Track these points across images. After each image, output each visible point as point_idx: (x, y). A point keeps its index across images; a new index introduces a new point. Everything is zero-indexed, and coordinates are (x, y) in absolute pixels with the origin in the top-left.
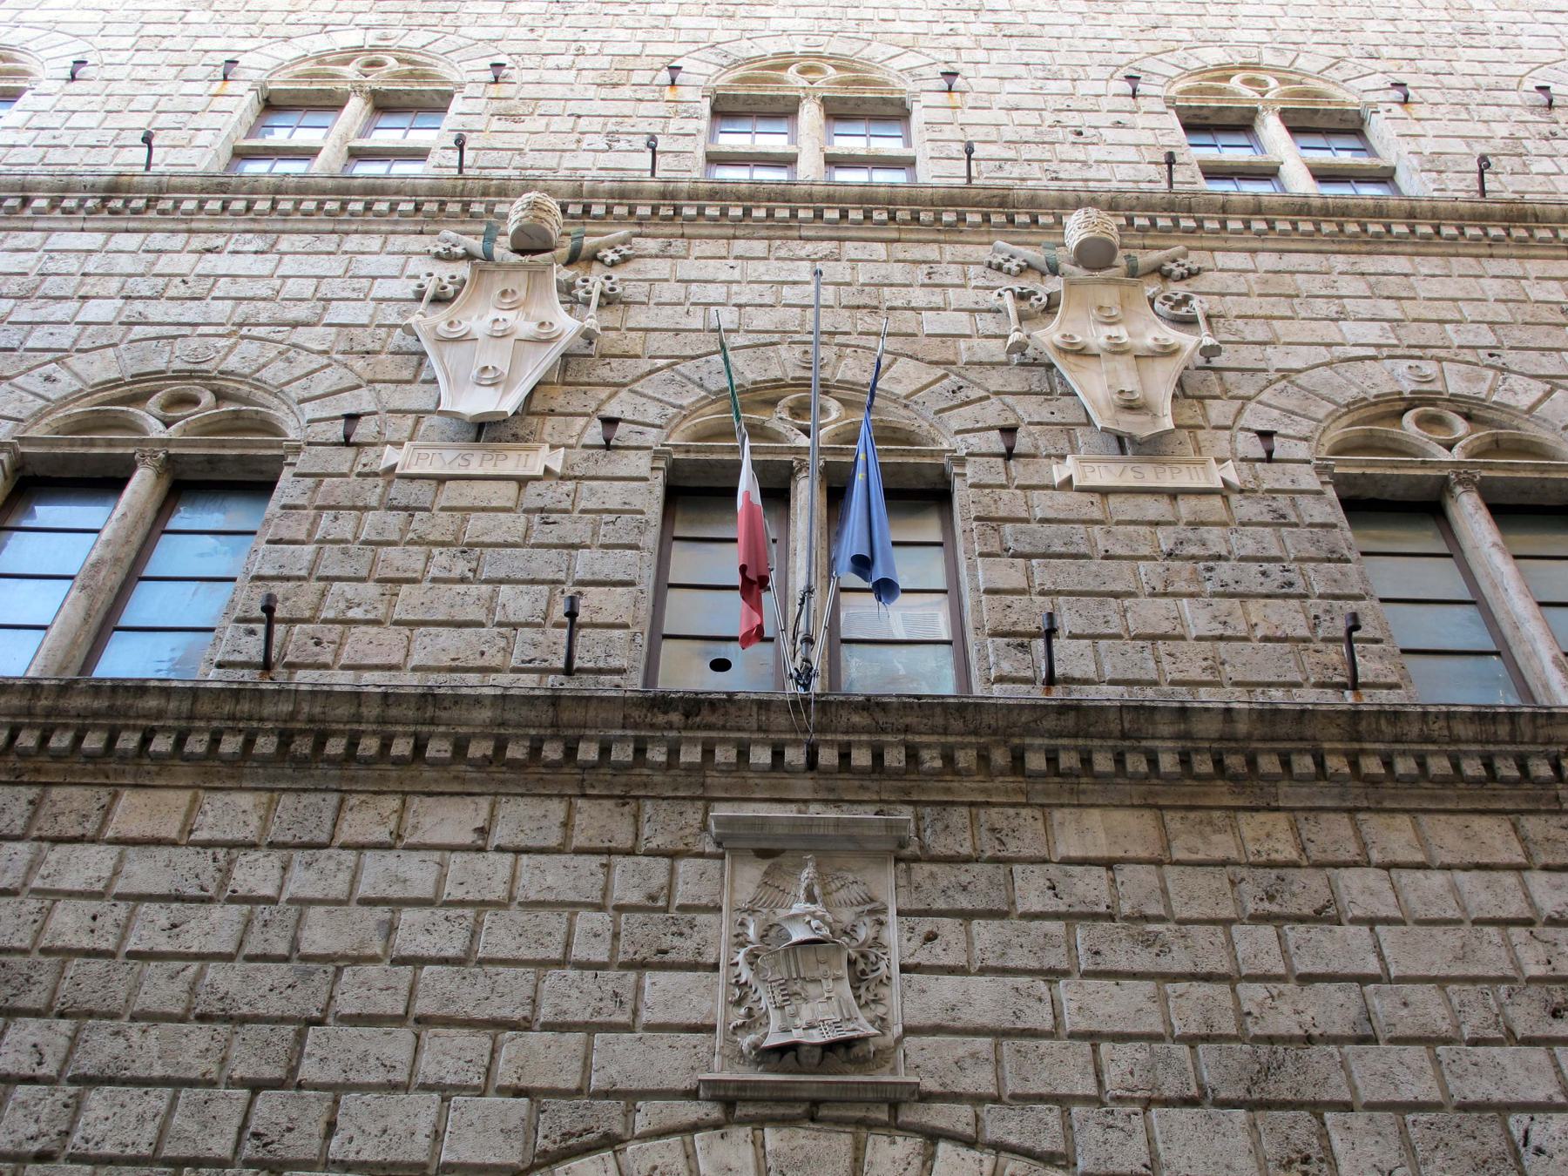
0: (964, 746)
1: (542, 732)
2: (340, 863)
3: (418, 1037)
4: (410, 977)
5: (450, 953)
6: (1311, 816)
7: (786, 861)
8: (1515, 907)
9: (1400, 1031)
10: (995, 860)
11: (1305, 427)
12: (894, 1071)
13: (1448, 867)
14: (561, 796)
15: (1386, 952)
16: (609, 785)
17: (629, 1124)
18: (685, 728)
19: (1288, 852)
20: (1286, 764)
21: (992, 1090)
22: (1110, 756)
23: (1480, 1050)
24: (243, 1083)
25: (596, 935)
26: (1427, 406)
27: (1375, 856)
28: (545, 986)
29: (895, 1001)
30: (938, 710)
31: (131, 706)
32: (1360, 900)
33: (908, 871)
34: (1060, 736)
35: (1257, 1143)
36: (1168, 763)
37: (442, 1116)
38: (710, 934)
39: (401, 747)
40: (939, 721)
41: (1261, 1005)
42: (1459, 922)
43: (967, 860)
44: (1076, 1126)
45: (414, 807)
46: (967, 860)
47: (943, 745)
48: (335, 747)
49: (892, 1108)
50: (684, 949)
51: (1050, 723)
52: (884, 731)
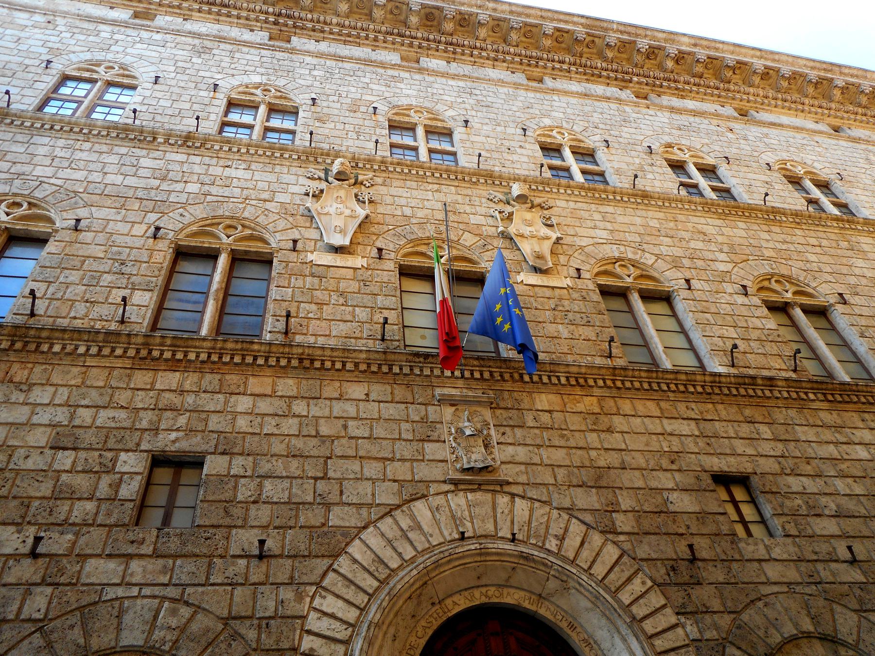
5: (366, 436)
9: (633, 467)
10: (517, 409)
16: (403, 380)
24: (311, 478)
48: (317, 364)
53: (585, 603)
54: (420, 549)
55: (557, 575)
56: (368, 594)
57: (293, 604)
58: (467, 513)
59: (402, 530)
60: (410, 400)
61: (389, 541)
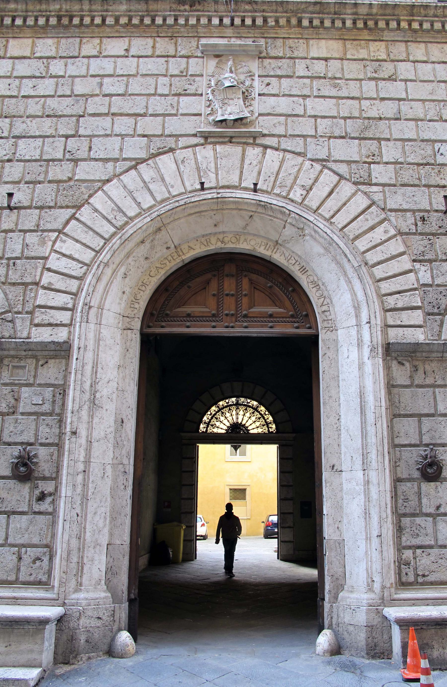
0: (282, 17)
1: (143, 13)
2: (83, 63)
3: (113, 120)
4: (109, 100)
5: (120, 92)
6: (393, 43)
7: (223, 58)
9: (407, 117)
10: (290, 58)
12: (255, 128)
13: (434, 63)
14: (151, 37)
15: (408, 91)
16: (167, 32)
17: (177, 145)
18: (191, 11)
19: (384, 56)
20: (387, 24)
21: (284, 133)
22: (330, 21)
23: (431, 123)
24: (63, 136)
25: (165, 85)
27: (411, 58)
28: (150, 102)
29: (257, 105)
30: (274, 4)
31: (6, 8)
32: (404, 73)
33: (262, 61)
34: (314, 13)
35: (360, 150)
36: (349, 23)
37: (122, 144)
38: (200, 84)
39: (98, 21)
40: (274, 8)
41: (367, 107)
42: (433, 81)
43: (281, 58)
44: (308, 144)
45: (104, 42)
46: (281, 58)
47: (276, 17)
48: (76, 21)
49: (254, 139)
50: (192, 89)
51: (311, 9)
52: (256, 11)
53: (318, 249)
54: (159, 199)
55: (294, 223)
56: (104, 239)
57: (36, 247)
58: (213, 165)
59: (145, 182)
60: (172, 53)
61: (130, 193)
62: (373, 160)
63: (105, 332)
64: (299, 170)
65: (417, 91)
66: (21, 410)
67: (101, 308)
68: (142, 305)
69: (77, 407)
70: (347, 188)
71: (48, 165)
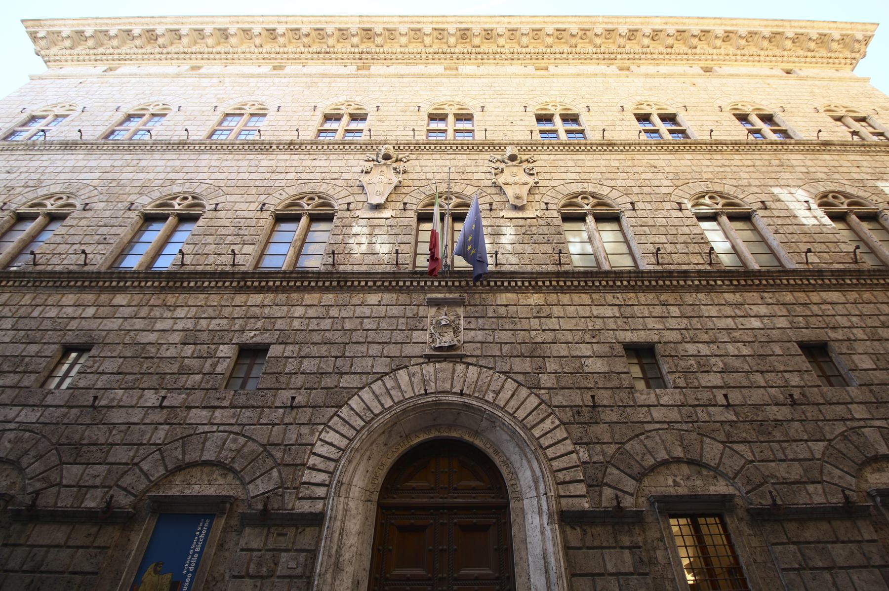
8: (588, 314)
11: (556, 201)
26: (584, 195)
50: (420, 326)
53: (506, 437)
58: (433, 377)
61: (377, 397)
62: (541, 371)
63: (351, 504)
64: (490, 381)
65: (567, 324)
66: (278, 573)
67: (350, 484)
68: (380, 480)
69: (323, 570)
70: (524, 392)
71: (322, 377)
